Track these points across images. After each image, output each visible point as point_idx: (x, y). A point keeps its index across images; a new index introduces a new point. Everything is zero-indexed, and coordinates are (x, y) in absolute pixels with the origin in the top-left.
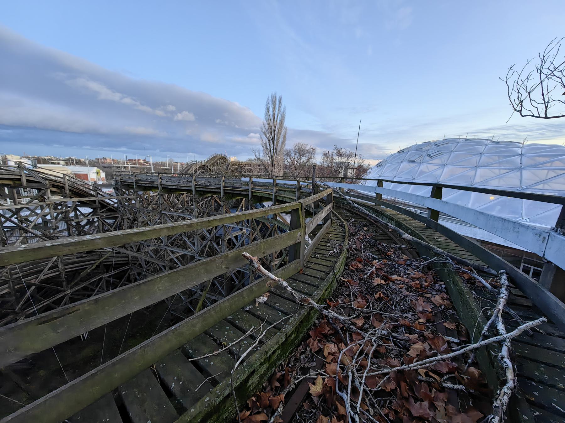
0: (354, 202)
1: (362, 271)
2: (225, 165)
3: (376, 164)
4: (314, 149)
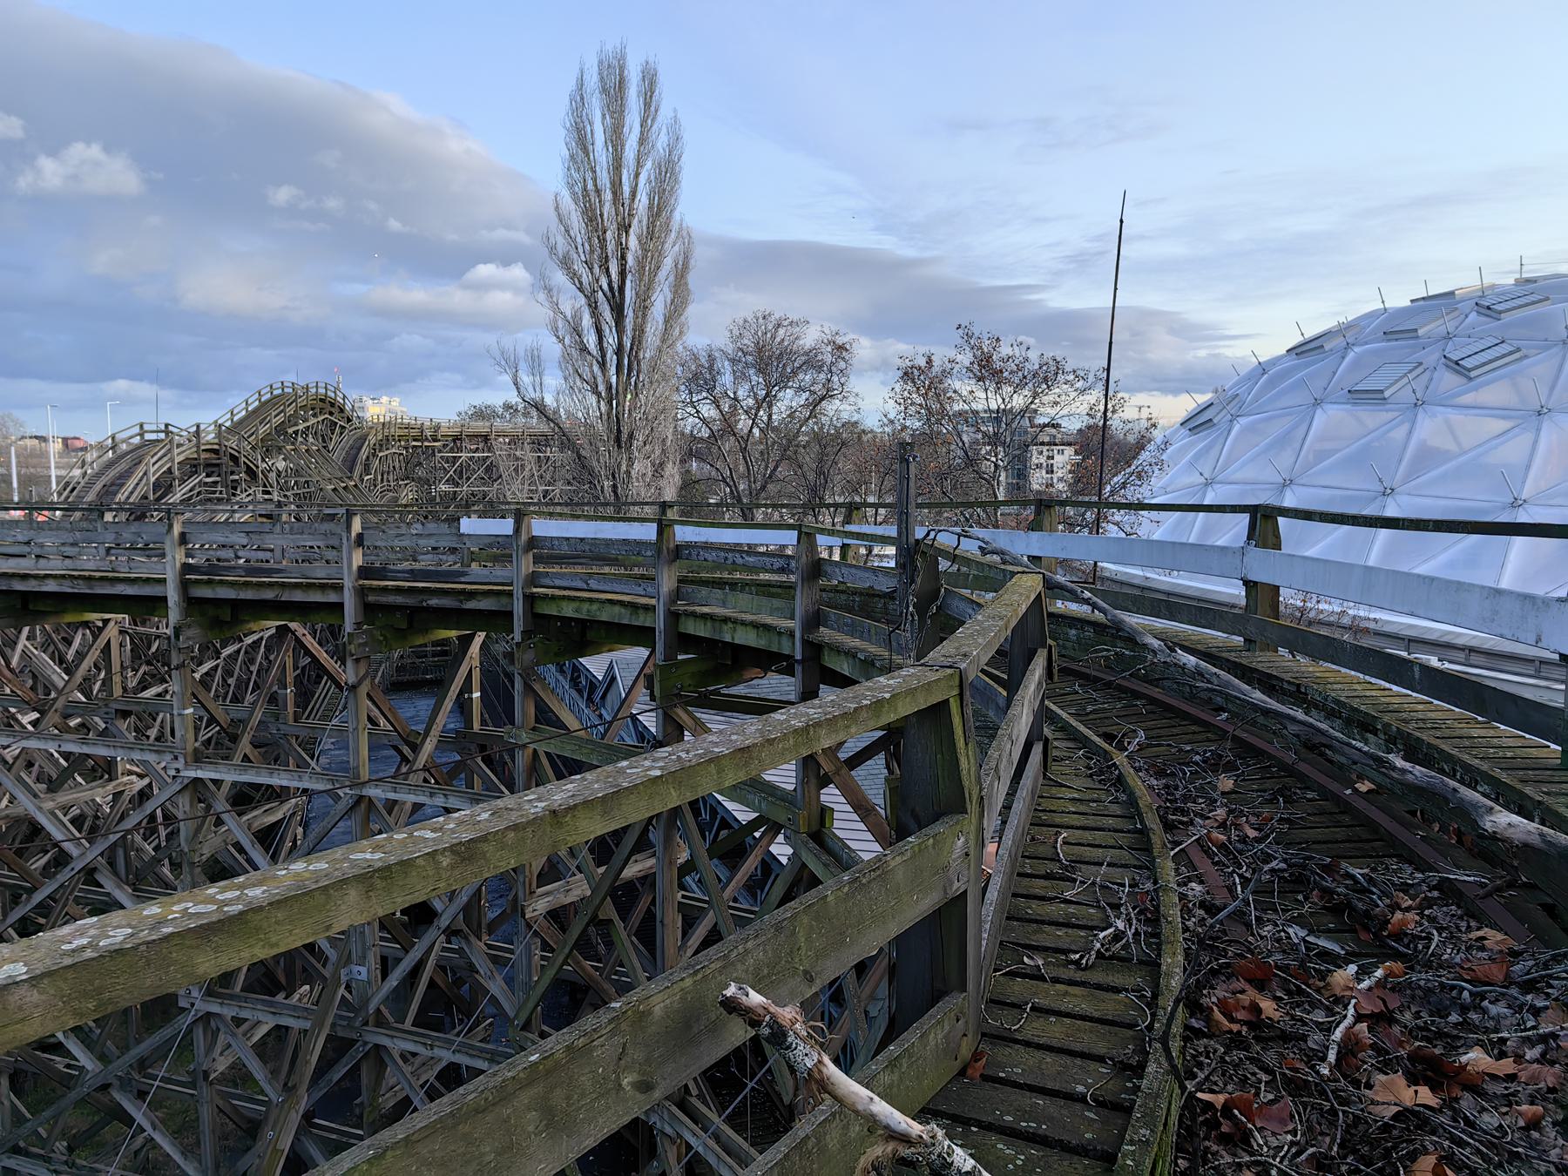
0: (1172, 644)
1: (1285, 1037)
2: (339, 446)
3: (1182, 415)
4: (841, 348)
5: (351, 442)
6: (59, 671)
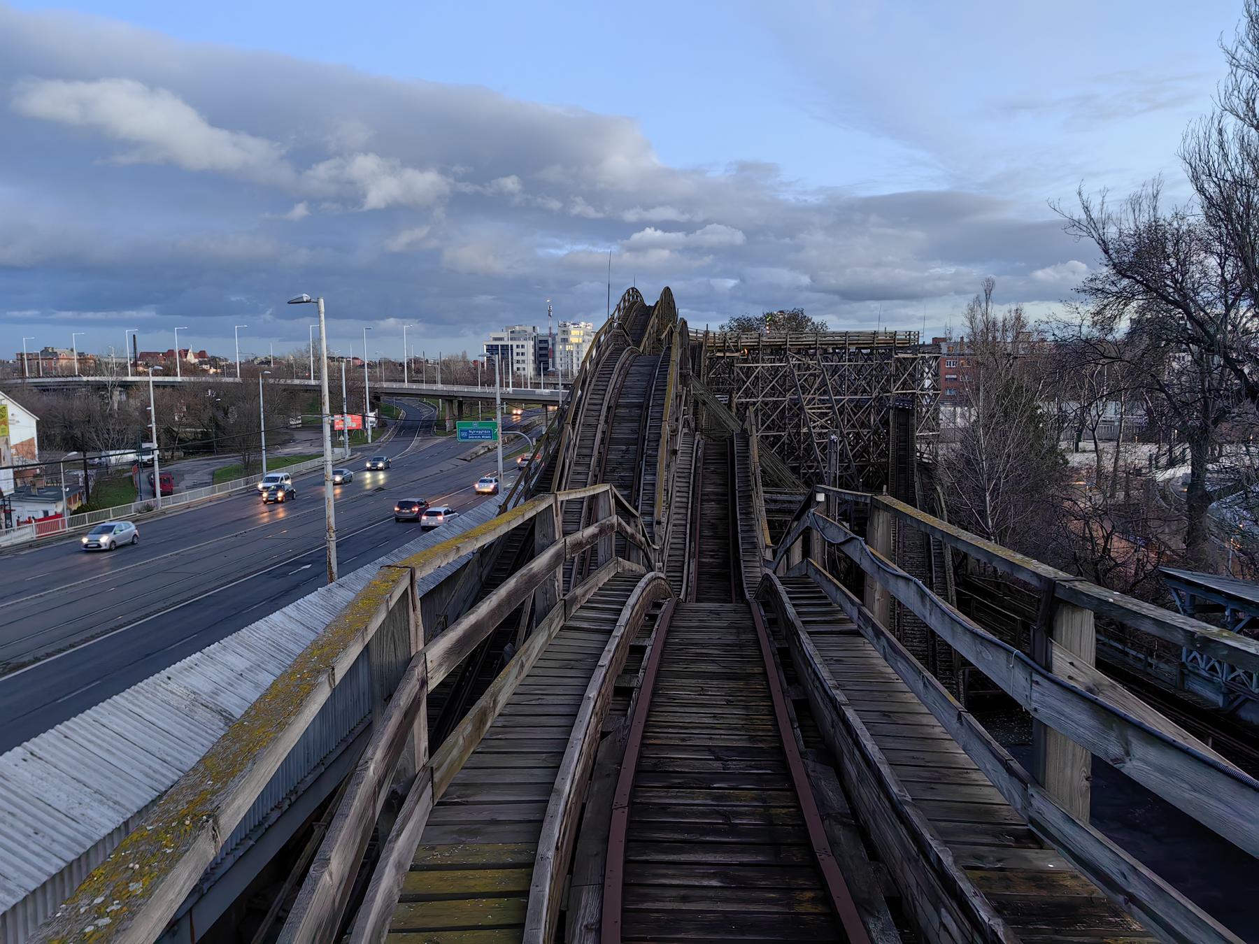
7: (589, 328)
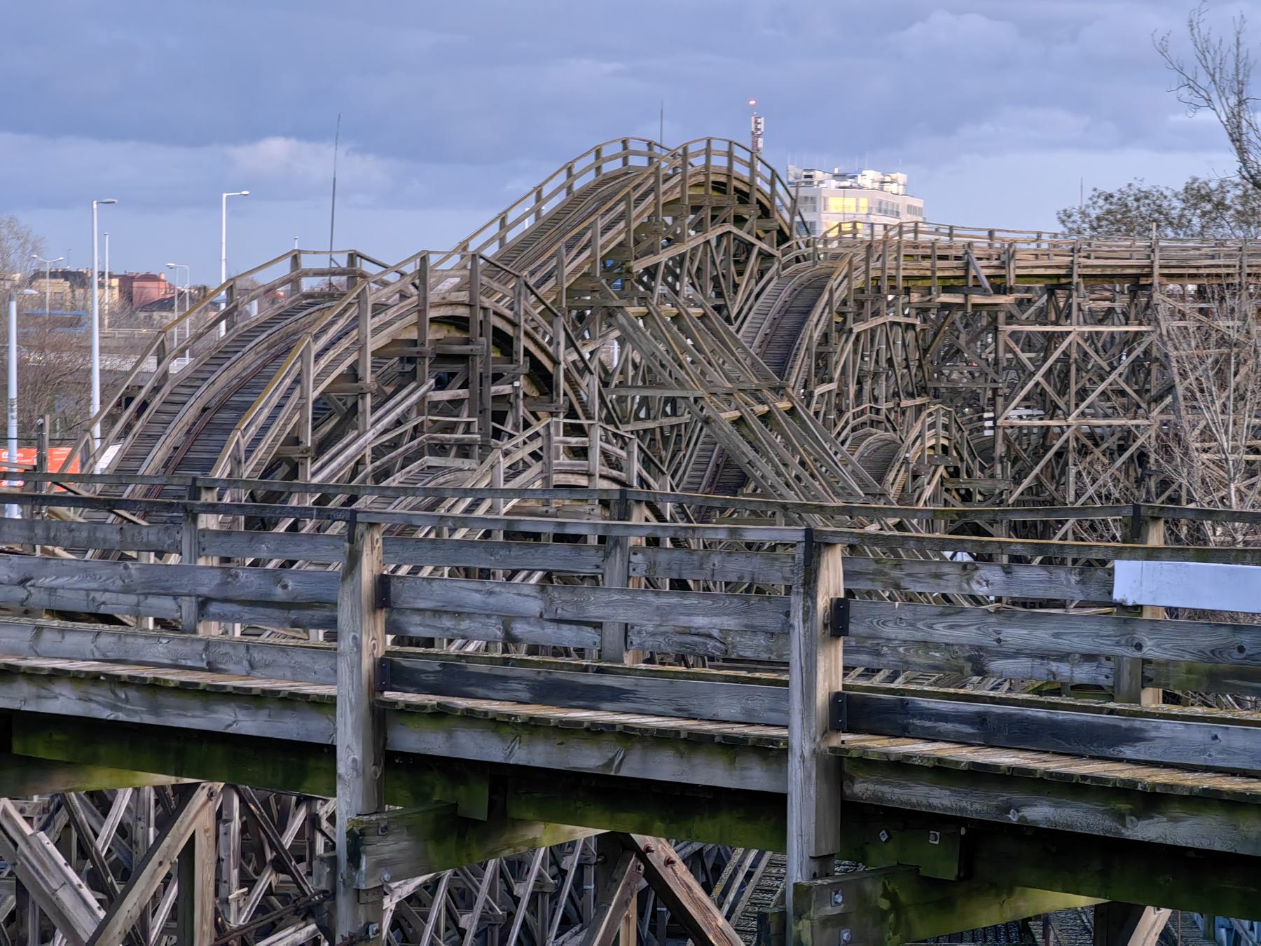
5: (784, 296)
6: (76, 880)
7: (893, 188)
